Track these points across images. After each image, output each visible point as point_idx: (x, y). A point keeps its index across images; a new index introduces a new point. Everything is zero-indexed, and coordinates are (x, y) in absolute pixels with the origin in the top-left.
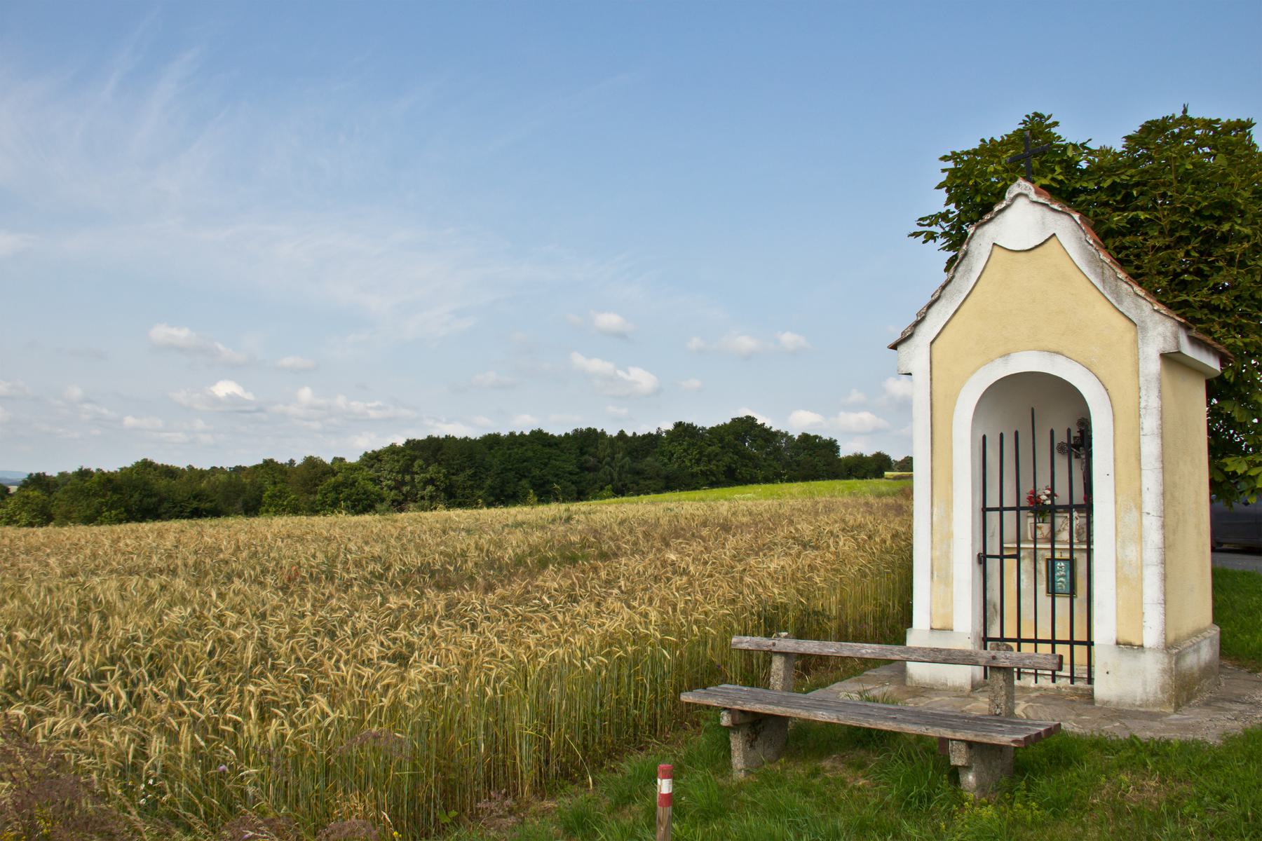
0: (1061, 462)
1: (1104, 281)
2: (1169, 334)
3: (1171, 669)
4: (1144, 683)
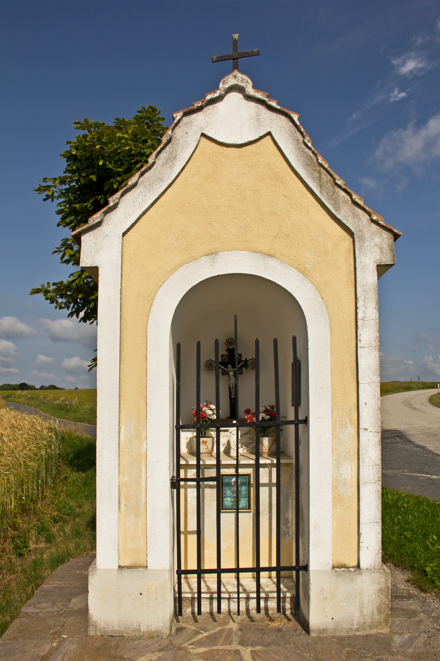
0: (208, 380)
1: (321, 186)
2: (385, 246)
3: (388, 588)
4: (362, 606)
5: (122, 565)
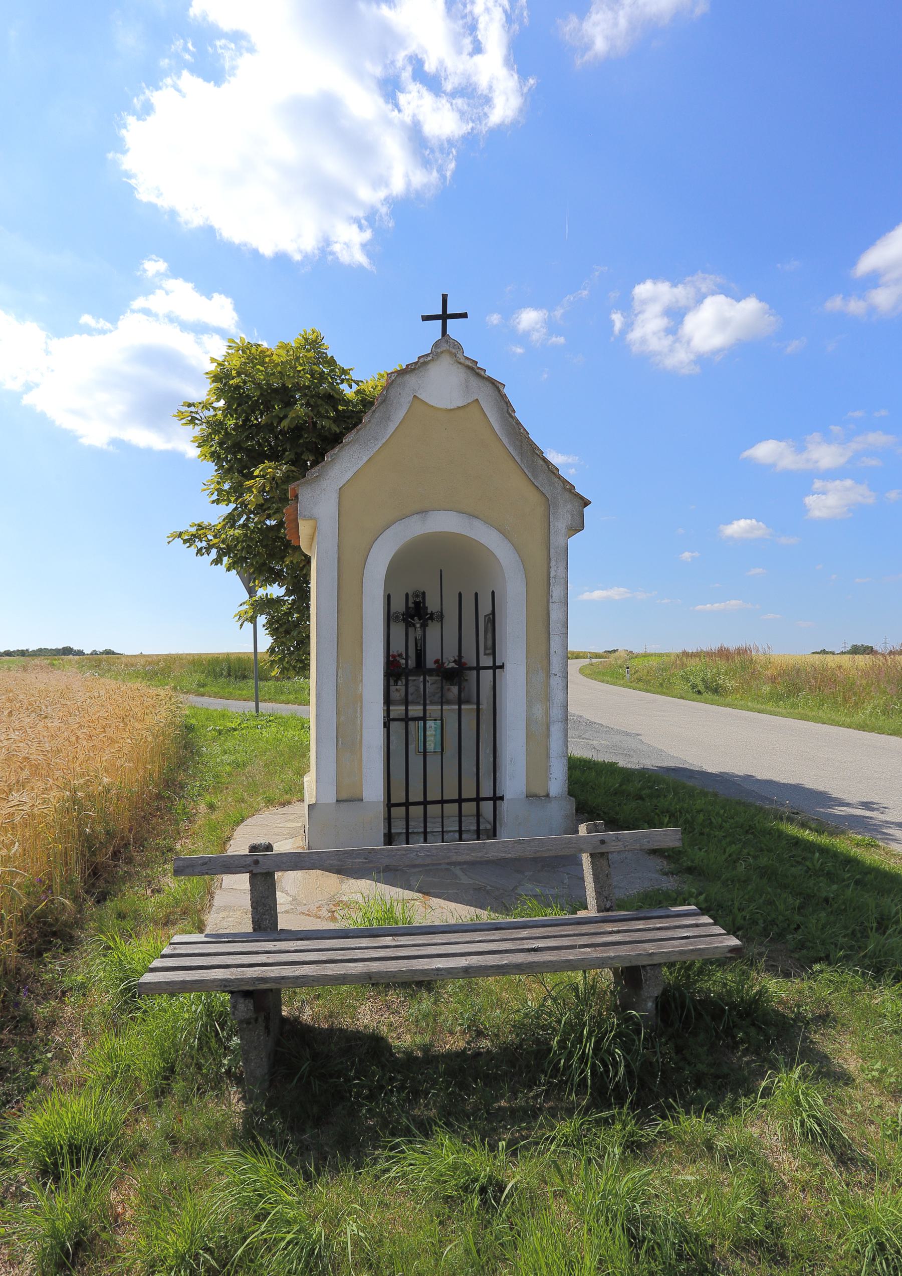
5: (340, 799)
